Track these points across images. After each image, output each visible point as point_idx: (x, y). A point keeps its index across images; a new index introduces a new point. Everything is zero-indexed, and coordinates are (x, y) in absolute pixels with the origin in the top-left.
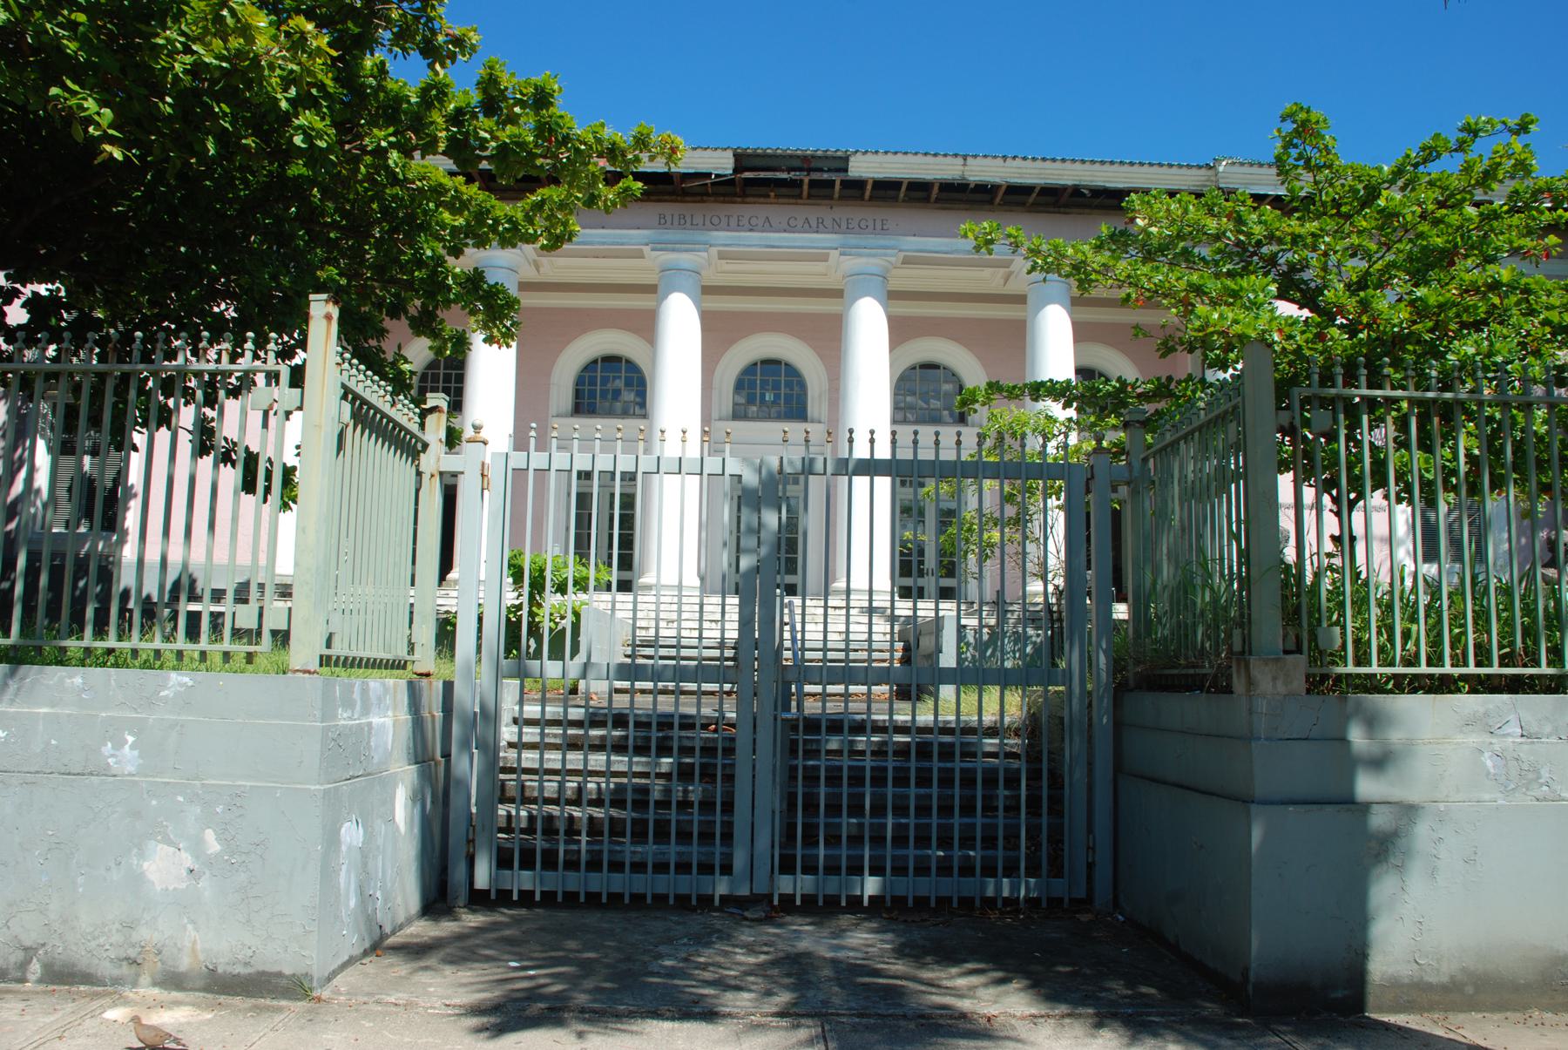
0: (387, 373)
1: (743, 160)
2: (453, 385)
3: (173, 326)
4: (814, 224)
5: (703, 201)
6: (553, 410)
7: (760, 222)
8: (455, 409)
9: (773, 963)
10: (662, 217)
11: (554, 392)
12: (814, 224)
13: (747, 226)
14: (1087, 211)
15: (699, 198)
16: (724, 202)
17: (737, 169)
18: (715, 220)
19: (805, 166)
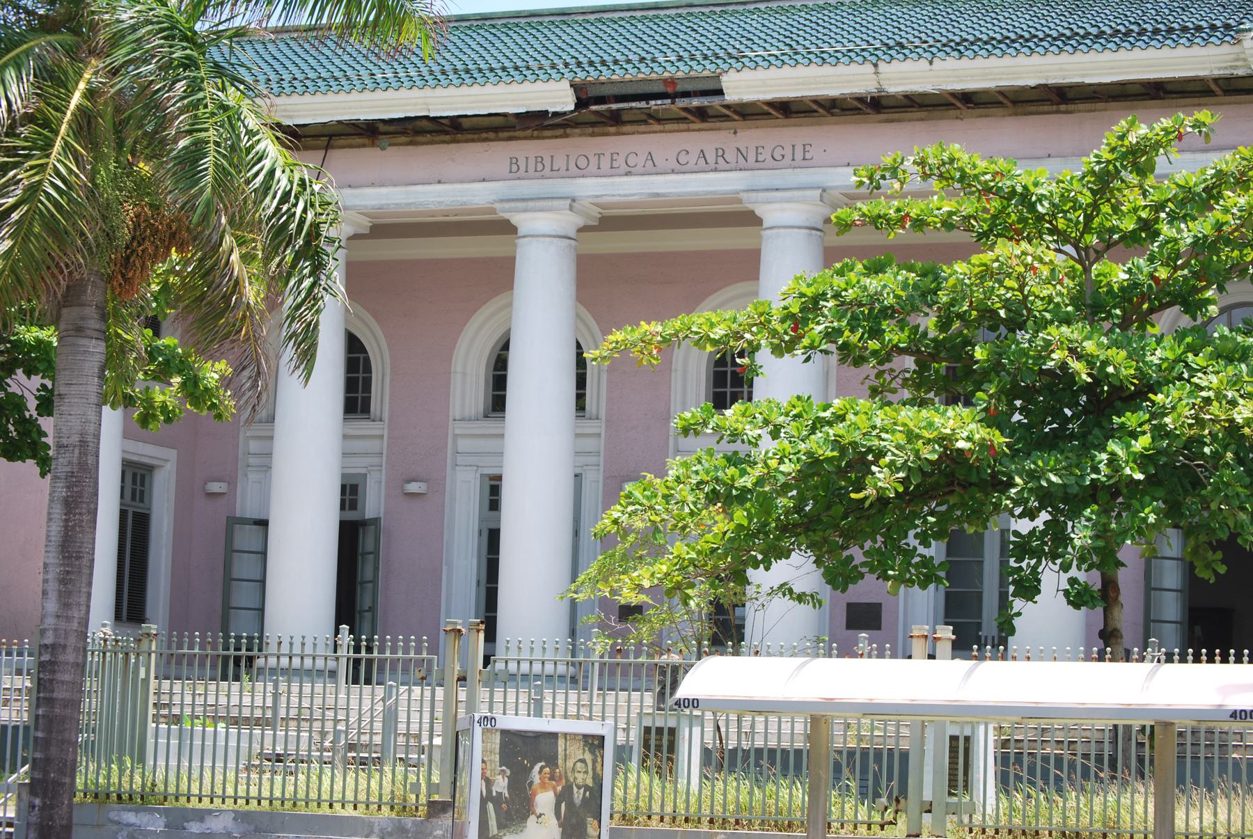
0: (206, 637)
1: (585, 96)
2: (361, 375)
3: (1218, 651)
4: (711, 157)
5: (566, 136)
6: (456, 410)
7: (641, 160)
8: (494, 410)
9: (84, 305)
10: (514, 161)
11: (456, 381)
12: (711, 157)
13: (624, 168)
14: (1101, 105)
15: (560, 132)
16: (593, 135)
17: (581, 103)
18: (582, 162)
19: (670, 90)
